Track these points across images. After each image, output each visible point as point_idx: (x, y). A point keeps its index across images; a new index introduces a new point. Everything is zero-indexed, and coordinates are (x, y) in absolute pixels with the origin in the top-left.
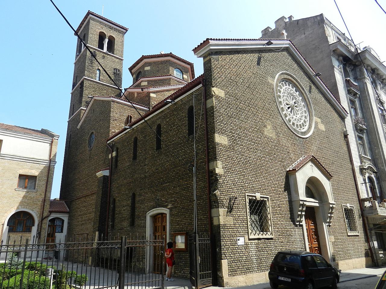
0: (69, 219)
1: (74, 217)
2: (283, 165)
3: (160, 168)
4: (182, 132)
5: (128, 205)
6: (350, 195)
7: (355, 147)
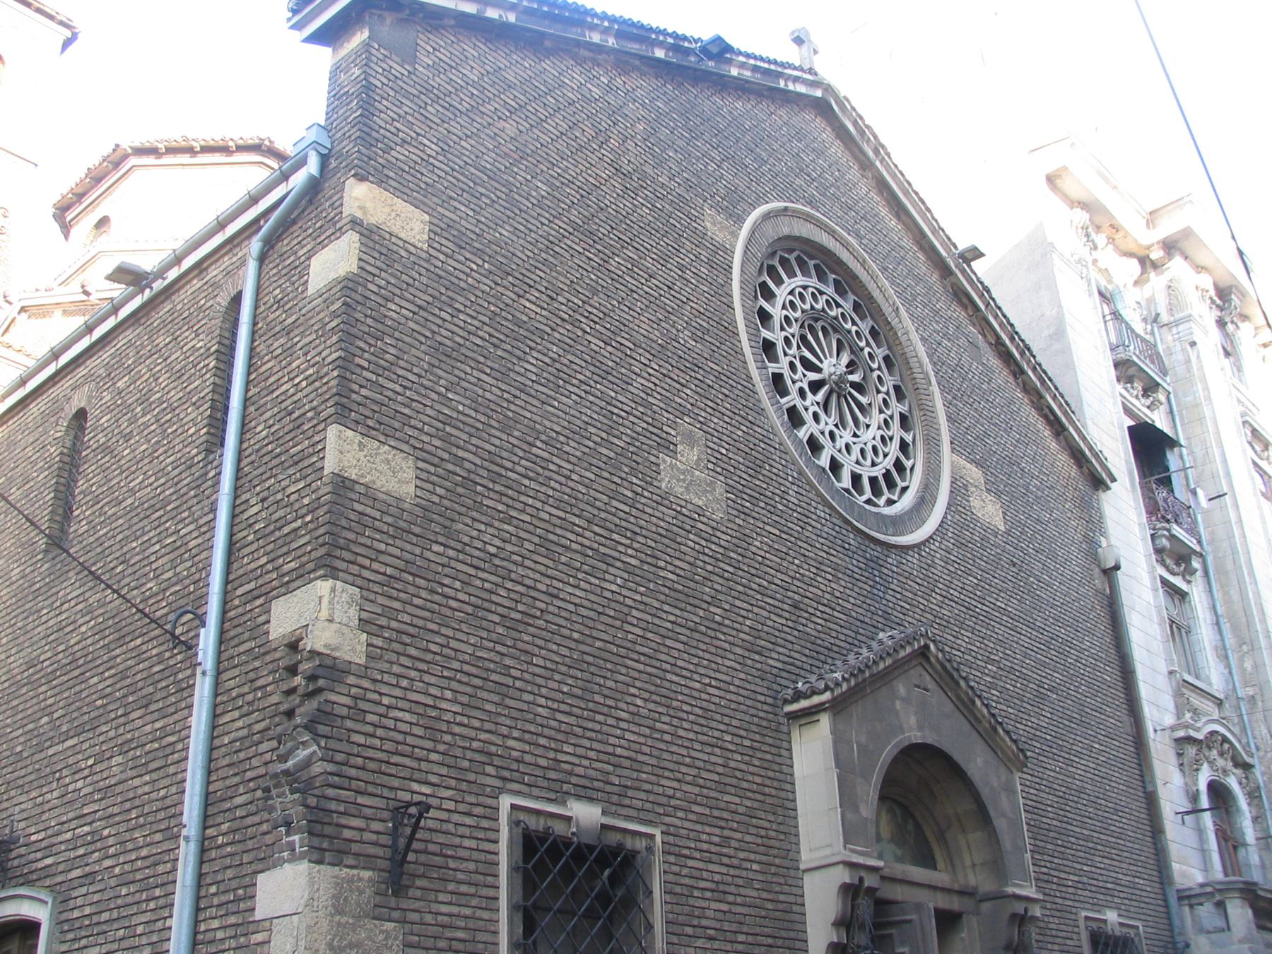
2: (758, 666)
6: (1123, 865)
7: (1125, 577)
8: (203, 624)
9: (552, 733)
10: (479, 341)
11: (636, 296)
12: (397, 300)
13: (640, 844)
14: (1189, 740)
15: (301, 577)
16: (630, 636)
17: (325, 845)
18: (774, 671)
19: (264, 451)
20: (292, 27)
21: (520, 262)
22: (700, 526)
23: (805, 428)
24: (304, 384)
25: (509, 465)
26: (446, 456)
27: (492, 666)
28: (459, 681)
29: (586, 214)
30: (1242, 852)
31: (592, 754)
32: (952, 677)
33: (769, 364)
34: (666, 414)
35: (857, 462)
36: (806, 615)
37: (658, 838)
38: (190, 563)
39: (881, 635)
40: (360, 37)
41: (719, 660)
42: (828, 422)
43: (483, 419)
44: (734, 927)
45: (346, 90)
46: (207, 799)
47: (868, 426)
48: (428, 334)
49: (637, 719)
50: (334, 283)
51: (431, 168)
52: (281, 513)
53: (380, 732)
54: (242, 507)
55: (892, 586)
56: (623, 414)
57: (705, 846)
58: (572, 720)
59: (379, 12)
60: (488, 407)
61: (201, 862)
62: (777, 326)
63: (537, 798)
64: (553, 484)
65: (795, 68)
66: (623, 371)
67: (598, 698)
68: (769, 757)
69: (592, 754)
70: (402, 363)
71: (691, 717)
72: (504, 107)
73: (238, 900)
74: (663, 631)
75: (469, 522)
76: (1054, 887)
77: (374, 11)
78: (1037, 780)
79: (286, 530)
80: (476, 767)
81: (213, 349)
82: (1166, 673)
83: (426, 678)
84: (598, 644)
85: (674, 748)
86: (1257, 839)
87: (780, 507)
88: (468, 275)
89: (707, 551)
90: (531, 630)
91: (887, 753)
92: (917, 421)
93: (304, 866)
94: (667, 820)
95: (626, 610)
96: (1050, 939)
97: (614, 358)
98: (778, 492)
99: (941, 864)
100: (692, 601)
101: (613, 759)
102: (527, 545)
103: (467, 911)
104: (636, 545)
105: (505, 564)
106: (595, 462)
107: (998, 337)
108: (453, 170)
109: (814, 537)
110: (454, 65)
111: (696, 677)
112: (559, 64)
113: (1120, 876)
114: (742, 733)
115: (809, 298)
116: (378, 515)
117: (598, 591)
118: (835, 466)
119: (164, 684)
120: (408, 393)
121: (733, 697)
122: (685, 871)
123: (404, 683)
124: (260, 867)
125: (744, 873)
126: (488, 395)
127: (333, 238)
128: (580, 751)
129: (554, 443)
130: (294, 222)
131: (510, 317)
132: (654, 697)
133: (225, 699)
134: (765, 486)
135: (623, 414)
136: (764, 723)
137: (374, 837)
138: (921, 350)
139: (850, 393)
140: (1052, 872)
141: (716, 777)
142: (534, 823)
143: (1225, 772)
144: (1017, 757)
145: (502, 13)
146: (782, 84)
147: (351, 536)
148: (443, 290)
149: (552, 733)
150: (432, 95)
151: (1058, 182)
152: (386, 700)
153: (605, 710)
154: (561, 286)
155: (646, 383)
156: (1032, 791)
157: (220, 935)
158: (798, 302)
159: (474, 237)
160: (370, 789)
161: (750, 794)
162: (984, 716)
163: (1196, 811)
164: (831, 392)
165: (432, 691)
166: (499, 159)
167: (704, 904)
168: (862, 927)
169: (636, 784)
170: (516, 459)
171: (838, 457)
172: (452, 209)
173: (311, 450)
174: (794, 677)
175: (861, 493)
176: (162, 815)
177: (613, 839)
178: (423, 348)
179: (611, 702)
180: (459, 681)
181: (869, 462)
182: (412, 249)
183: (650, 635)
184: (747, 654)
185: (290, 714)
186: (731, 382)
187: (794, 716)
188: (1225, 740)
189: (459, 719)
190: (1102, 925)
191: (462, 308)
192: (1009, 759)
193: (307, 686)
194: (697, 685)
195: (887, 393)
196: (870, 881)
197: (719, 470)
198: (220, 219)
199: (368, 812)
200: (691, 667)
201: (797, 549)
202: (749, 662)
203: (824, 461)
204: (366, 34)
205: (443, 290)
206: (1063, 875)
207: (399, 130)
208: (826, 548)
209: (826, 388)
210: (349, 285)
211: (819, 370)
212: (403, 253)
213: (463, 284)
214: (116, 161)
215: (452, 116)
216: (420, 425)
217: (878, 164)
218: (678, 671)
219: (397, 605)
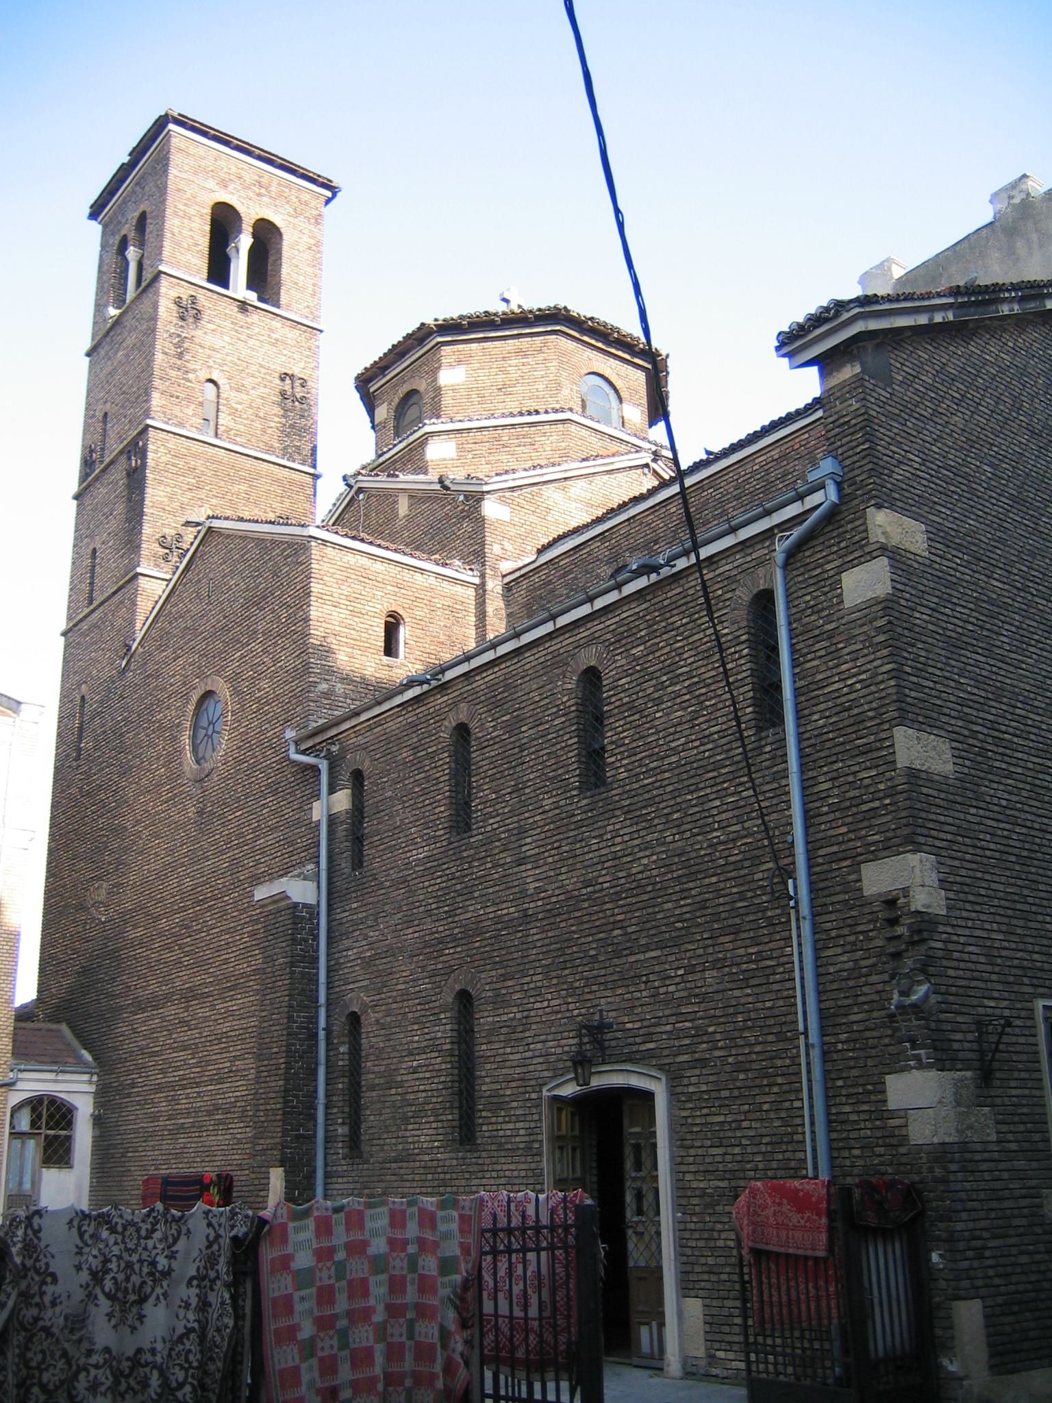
0: (98, 1104)
1: (129, 1095)
3: (608, 878)
4: (719, 714)
5: (434, 1047)
15: (889, 848)
19: (825, 737)
25: (1003, 728)
27: (1016, 898)
28: (999, 915)
29: (1018, 483)
40: (848, 372)
50: (873, 602)
52: (856, 793)
53: (962, 965)
54: (811, 782)
64: (1032, 737)
75: (987, 783)
79: (864, 808)
88: (956, 570)
93: (933, 1074)
108: (932, 476)
110: (914, 373)
112: (979, 341)
116: (935, 793)
123: (970, 924)
124: (886, 1070)
127: (862, 560)
157: (854, 1117)
159: (953, 533)
165: (987, 926)
172: (936, 513)
173: (878, 745)
180: (999, 915)
185: (897, 956)
193: (911, 936)
210: (887, 605)
212: (916, 565)
214: (421, 335)
219: (957, 863)
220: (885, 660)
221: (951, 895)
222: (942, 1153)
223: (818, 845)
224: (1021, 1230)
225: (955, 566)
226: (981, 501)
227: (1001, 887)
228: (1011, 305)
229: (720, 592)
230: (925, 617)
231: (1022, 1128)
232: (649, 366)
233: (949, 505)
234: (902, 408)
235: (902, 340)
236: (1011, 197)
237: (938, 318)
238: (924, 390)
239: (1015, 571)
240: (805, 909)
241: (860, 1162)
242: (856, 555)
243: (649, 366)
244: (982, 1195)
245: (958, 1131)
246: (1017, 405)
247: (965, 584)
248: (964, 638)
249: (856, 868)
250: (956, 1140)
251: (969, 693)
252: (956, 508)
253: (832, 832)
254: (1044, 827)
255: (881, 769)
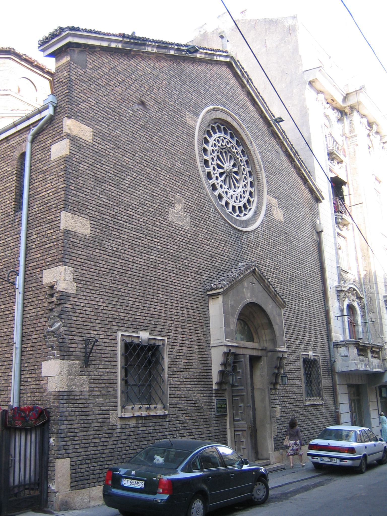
2: (199, 279)
6: (316, 336)
8: (18, 275)
9: (134, 309)
10: (110, 175)
11: (162, 150)
12: (83, 163)
13: (160, 343)
14: (342, 291)
15: (53, 264)
16: (158, 274)
17: (65, 354)
18: (204, 280)
19: (37, 216)
20: (41, 51)
21: (123, 143)
22: (182, 232)
23: (217, 191)
24: (51, 194)
25: (120, 218)
26: (100, 218)
27: (115, 289)
28: (105, 295)
29: (145, 120)
30: (356, 327)
31: (146, 315)
32: (263, 279)
33: (206, 169)
34: (171, 193)
35: (235, 202)
36: (215, 260)
37: (166, 341)
38: (10, 252)
39: (240, 264)
40: (66, 59)
41: (187, 278)
42: (225, 187)
43: (111, 203)
44: (189, 367)
45: (62, 80)
46: (22, 335)
47: (239, 187)
48: (93, 174)
49: (160, 302)
51: (92, 110)
53: (81, 315)
54: (30, 235)
55: (244, 246)
56: (157, 195)
57: (181, 342)
58: (140, 304)
59: (73, 49)
60: (113, 199)
61: (22, 355)
62: (209, 154)
63: (129, 331)
64: (134, 223)
65: (221, 51)
66: (157, 179)
67: (148, 296)
68: (202, 310)
69: (146, 315)
70: (85, 186)
71: (177, 299)
72: (117, 81)
73: (36, 369)
74: (169, 271)
75: (107, 240)
76: (292, 345)
77: (71, 48)
78: (289, 309)
79: (47, 246)
80: (111, 323)
81: (15, 172)
82: (336, 267)
83: (95, 296)
84: (148, 277)
85: (172, 310)
86: (362, 323)
87: (208, 222)
88: (106, 150)
89: (184, 241)
90: (127, 275)
91: (240, 307)
92: (256, 184)
93: (58, 361)
94: (169, 334)
95: (157, 265)
96: (290, 362)
97: (154, 175)
98: (208, 217)
99: (255, 340)
100: (178, 259)
101: (152, 316)
102: (126, 246)
103: (108, 370)
104: (161, 242)
105: (119, 253)
106: (148, 214)
107: (286, 149)
108: (100, 110)
109: (219, 232)
110: (99, 67)
111: (179, 285)
112: (136, 60)
113: (315, 339)
114: (193, 302)
115: (221, 141)
116: (78, 242)
117: (148, 259)
118: (227, 204)
119: (3, 293)
120: (87, 197)
121: (191, 291)
122: (174, 350)
123: (88, 298)
124: (43, 359)
125: (193, 349)
126: (113, 194)
127: (59, 140)
128: (142, 314)
129: (134, 209)
130: (44, 130)
131: (120, 164)
132: (166, 294)
133: (27, 302)
134: (203, 215)
135: (157, 195)
136: (201, 298)
137: (79, 350)
138: (259, 157)
139: (233, 176)
140: (292, 340)
141: (184, 318)
142: (128, 340)
143: (353, 301)
144: (283, 304)
145: (116, 44)
146: (215, 58)
147: (70, 250)
148: (98, 157)
149: (134, 309)
150: (92, 81)
151: (313, 84)
152: (82, 305)
153: (150, 300)
154: (137, 150)
155: (165, 183)
156: (287, 313)
157: (29, 380)
158: (217, 143)
159: (107, 135)
160: (78, 334)
161: (195, 323)
162: (272, 291)
163: (343, 316)
164: (227, 176)
165: (97, 300)
166: (116, 103)
167: (180, 360)
168: (230, 365)
169: (160, 323)
170: (122, 216)
171: (228, 201)
172: (100, 125)
173: (55, 219)
174: (210, 282)
175: (235, 212)
176: (5, 338)
177: (152, 342)
178: (92, 179)
179: (152, 297)
180: (105, 295)
181: (238, 201)
182: (87, 143)
183: (165, 272)
184: (195, 275)
185: (51, 310)
186: (193, 178)
187: (210, 295)
188: (354, 290)
189: (105, 308)
190: (307, 356)
191: (104, 163)
192: (280, 305)
193: (57, 302)
194: (179, 288)
195: (246, 174)
196: (233, 350)
197: (188, 211)
198: (15, 123)
199: (77, 342)
200: (178, 282)
201: (213, 236)
202: (196, 278)
203: (223, 203)
204: (69, 58)
205: (98, 157)
206: (295, 341)
207: (81, 96)
208: (223, 235)
209: (225, 174)
210: (66, 159)
211: (222, 168)
212: (84, 145)
213: (104, 154)
215: (99, 88)
216: (91, 208)
217: (248, 86)
218: (173, 283)
219: (85, 272)
220: (62, 183)
221: (79, 285)
222: (59, 395)
223: (29, 262)
224: (97, 428)
225: (106, 148)
226: (124, 124)
227: (108, 284)
228: (153, 49)
229: (9, 153)
230: (85, 167)
231: (103, 385)
232: (51, 79)
233: (107, 123)
234: (89, 79)
235: (95, 52)
236: (200, 31)
237: (113, 45)
238: (103, 74)
239: (137, 155)
240: (21, 290)
241: (30, 399)
242: (58, 137)
243: (51, 79)
244: (77, 414)
245: (67, 386)
246: (151, 90)
247: (110, 157)
248: (105, 179)
249: (41, 272)
250: (66, 390)
251: (104, 202)
252: (111, 125)
253: (35, 257)
254: (134, 261)
255: (55, 230)
